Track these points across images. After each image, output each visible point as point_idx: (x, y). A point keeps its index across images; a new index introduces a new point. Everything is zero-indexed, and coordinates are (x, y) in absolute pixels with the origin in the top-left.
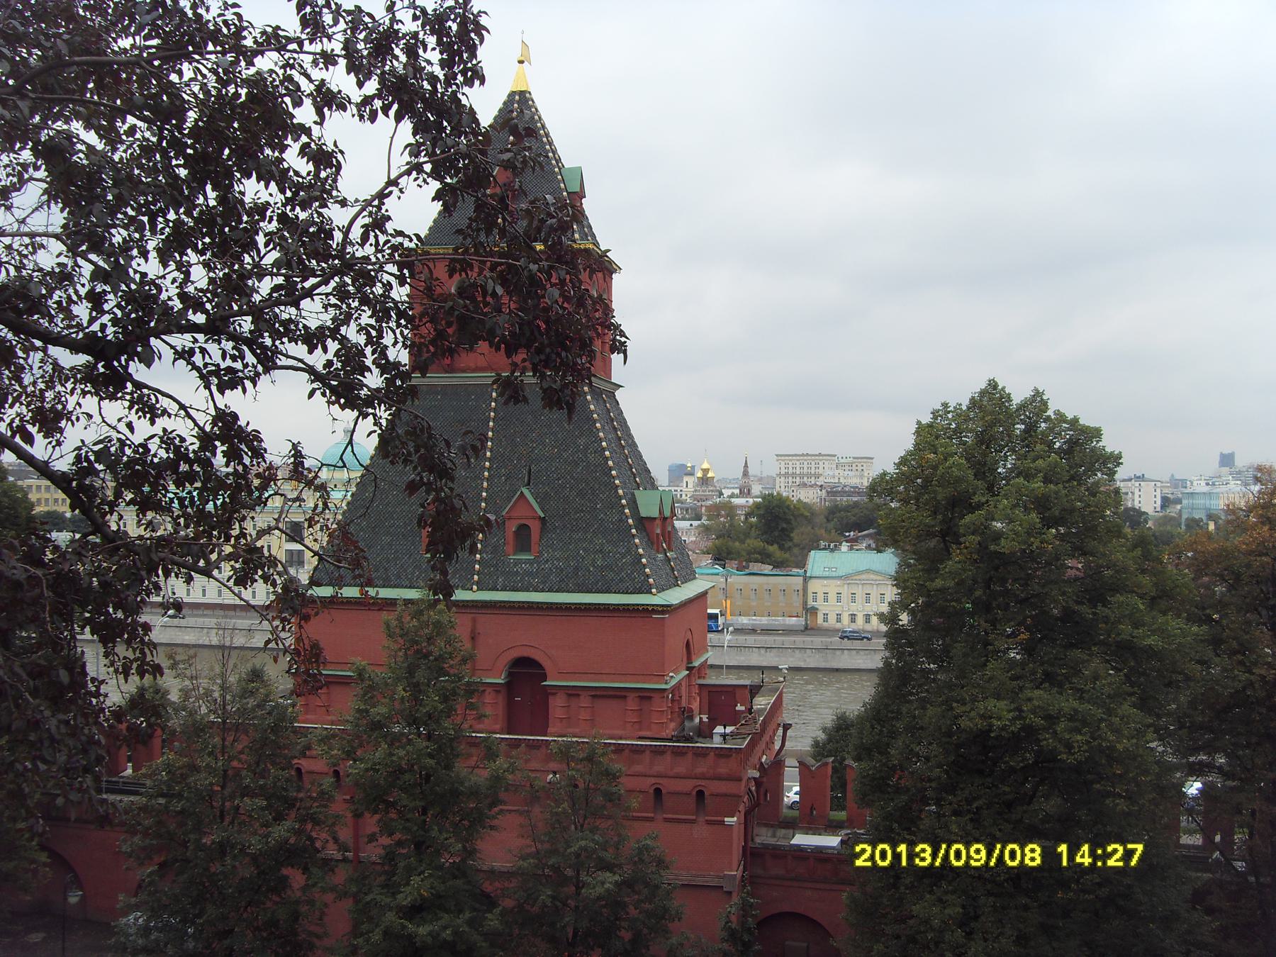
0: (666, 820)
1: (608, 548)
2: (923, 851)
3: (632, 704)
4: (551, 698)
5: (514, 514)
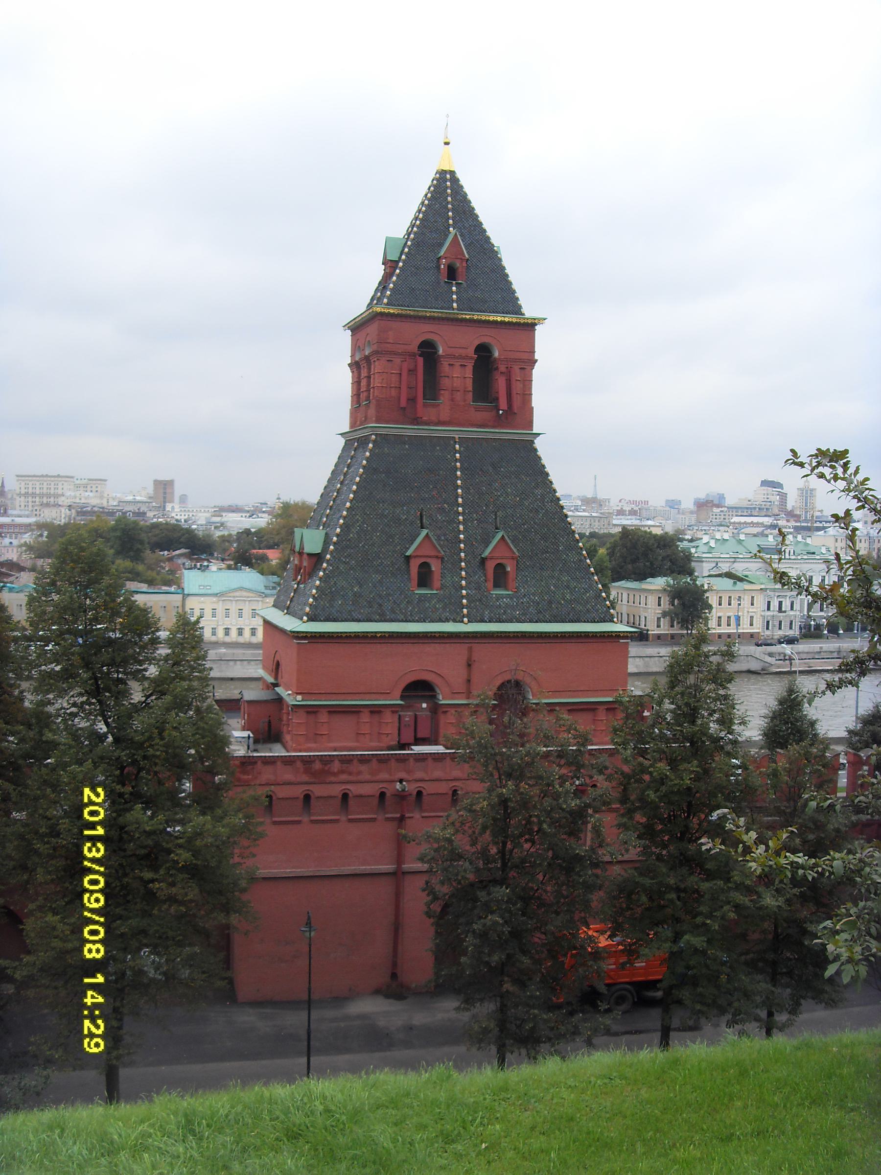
1: (573, 584)
2: (98, 850)
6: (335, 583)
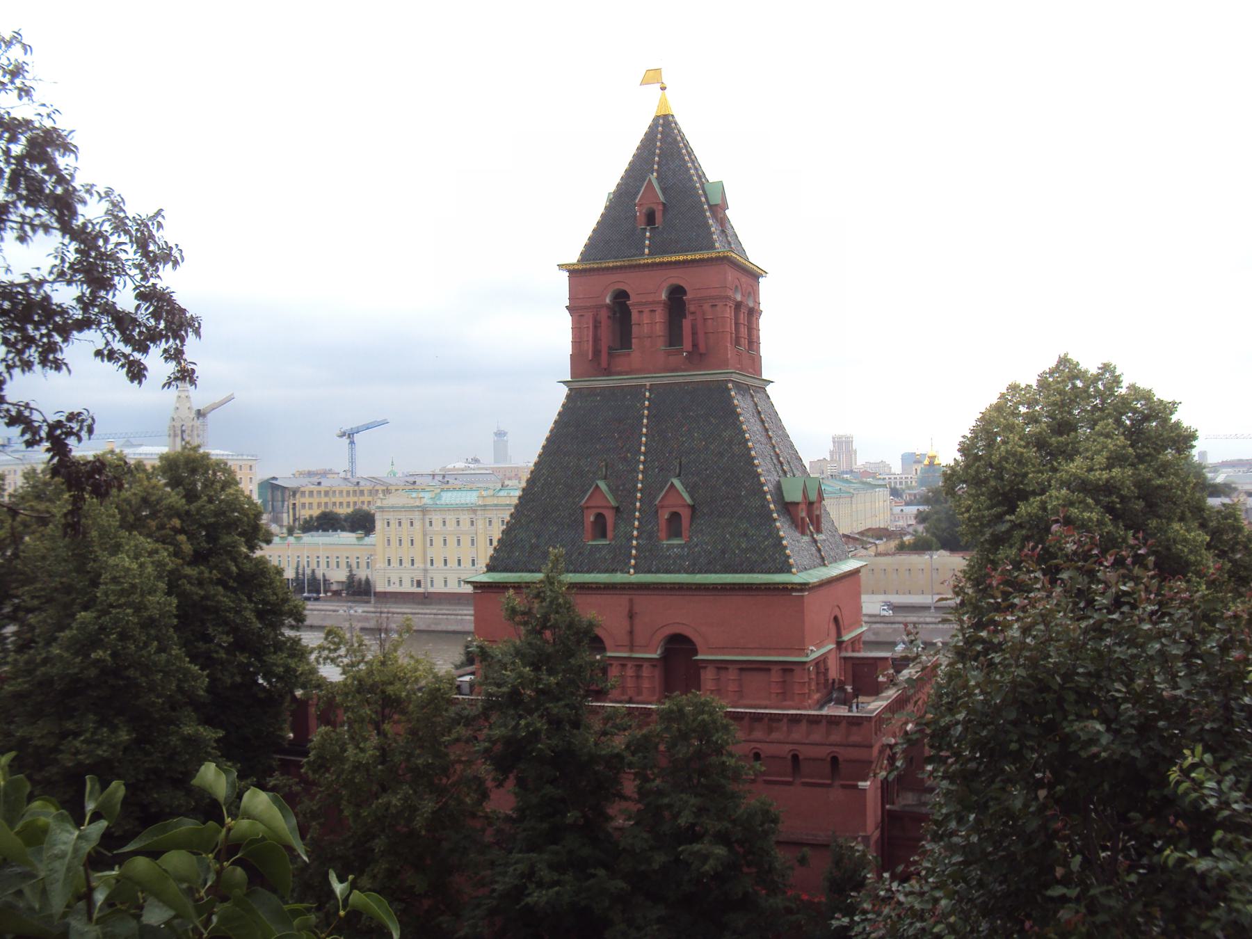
1: (751, 532)
3: (775, 676)
5: (591, 504)
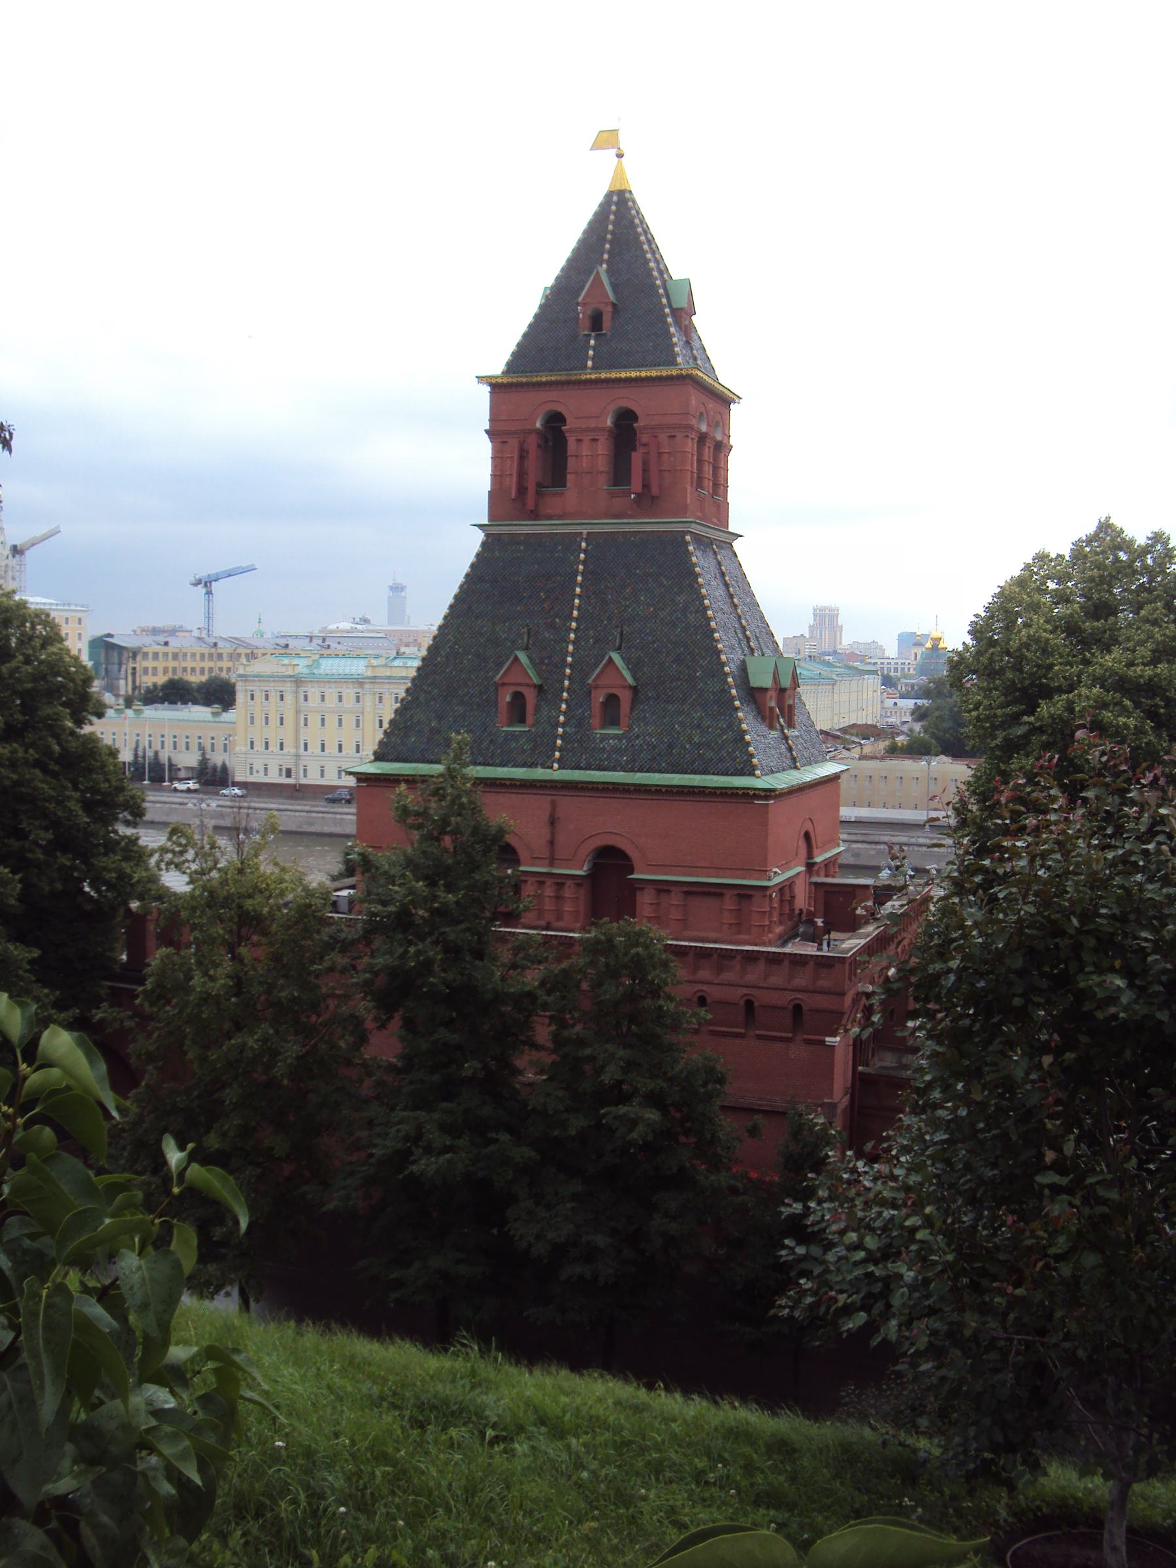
0: (759, 1037)
3: (729, 903)
4: (638, 893)
6: (412, 716)
